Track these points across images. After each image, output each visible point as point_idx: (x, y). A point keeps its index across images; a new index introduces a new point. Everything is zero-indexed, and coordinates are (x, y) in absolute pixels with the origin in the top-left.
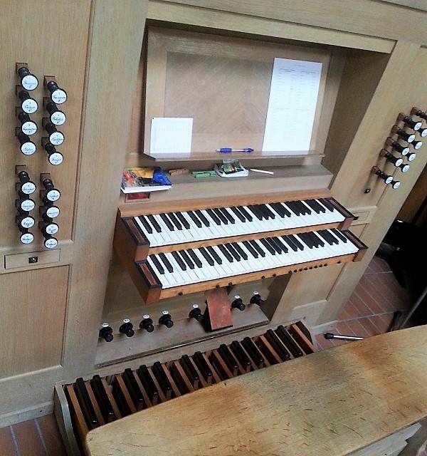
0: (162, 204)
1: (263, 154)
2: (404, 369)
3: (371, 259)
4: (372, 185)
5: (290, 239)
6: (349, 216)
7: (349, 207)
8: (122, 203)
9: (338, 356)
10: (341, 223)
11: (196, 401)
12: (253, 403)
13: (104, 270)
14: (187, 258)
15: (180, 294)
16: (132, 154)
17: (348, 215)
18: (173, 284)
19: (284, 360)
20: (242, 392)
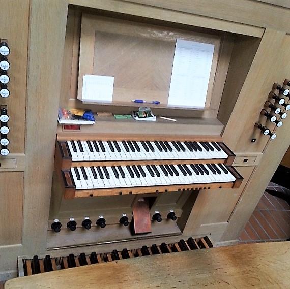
0: (89, 135)
1: (168, 106)
2: (261, 270)
4: (257, 136)
6: (231, 154)
7: (235, 151)
8: (60, 130)
9: (209, 254)
11: (91, 271)
12: (134, 278)
13: (49, 178)
14: (100, 170)
15: (91, 195)
16: (71, 99)
20: (128, 269)
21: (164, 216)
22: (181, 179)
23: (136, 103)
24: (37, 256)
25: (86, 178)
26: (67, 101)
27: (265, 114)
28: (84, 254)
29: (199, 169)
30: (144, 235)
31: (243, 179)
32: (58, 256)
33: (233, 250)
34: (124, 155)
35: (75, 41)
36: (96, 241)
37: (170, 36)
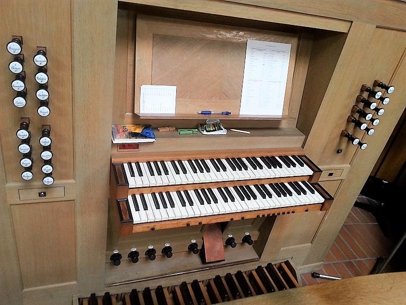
0: (149, 154)
3: (349, 211)
4: (343, 146)
5: (295, 186)
6: (317, 170)
8: (115, 151)
10: (311, 177)
14: (162, 197)
15: (153, 229)
17: (316, 169)
18: (144, 220)
19: (258, 294)
21: (238, 240)
22: (259, 204)
23: (203, 115)
24: (95, 294)
25: (146, 208)
26: (122, 116)
27: (353, 121)
28: (148, 288)
29: (280, 189)
30: (219, 264)
31: (333, 199)
32: (120, 292)
33: (328, 288)
34: (192, 177)
35: (129, 50)
36: (161, 273)
37: (239, 36)
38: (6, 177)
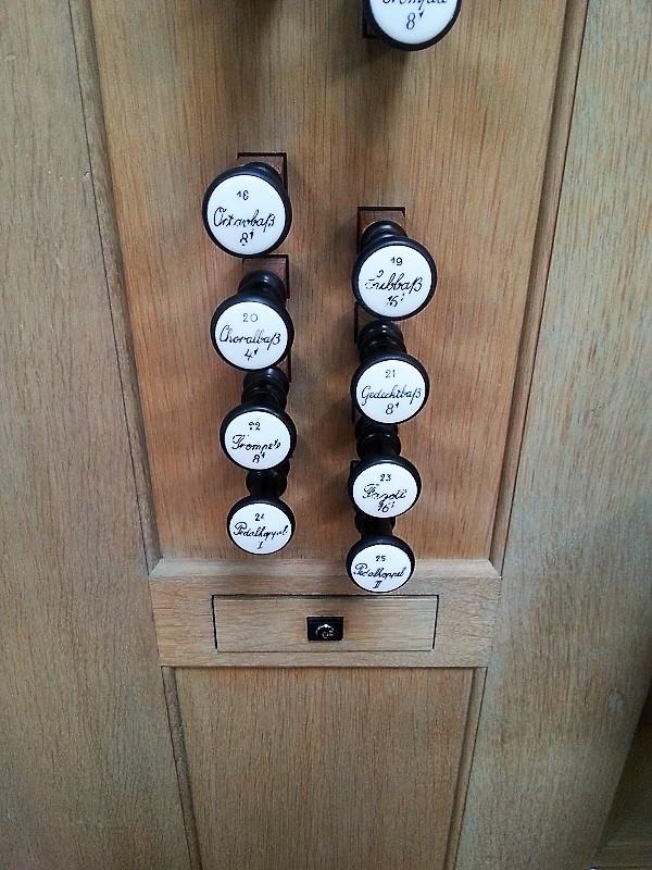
38: (154, 527)
